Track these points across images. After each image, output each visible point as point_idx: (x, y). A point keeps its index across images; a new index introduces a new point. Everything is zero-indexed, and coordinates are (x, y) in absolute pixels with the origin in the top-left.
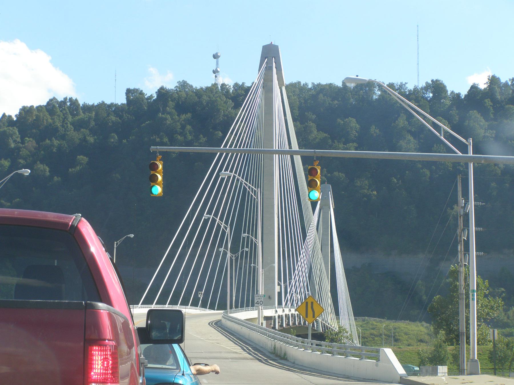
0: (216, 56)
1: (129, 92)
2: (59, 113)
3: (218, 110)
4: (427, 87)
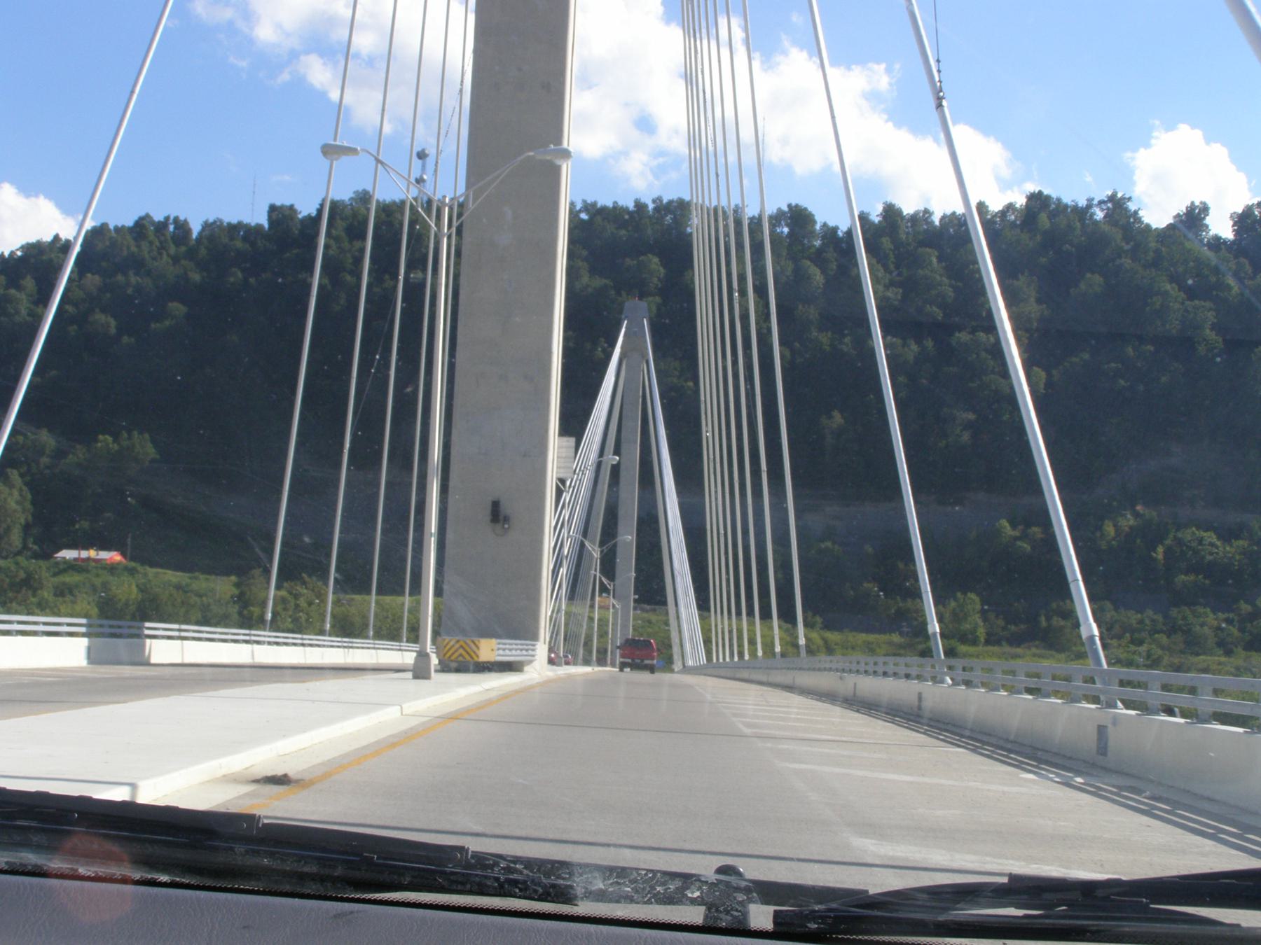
1: (273, 209)
2: (152, 237)
4: (777, 219)
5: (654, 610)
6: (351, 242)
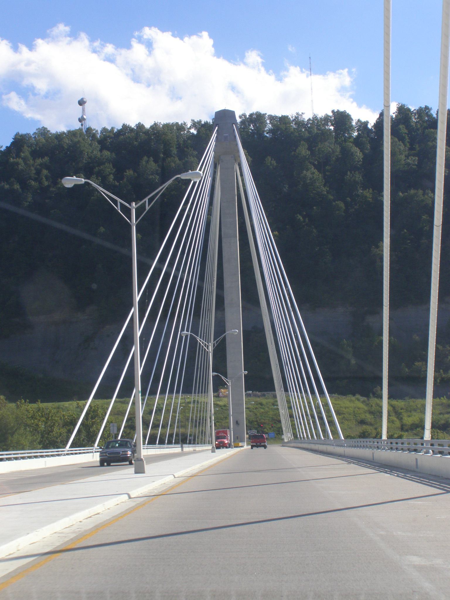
0: (81, 103)
3: (81, 152)
5: (264, 395)
6: (34, 159)
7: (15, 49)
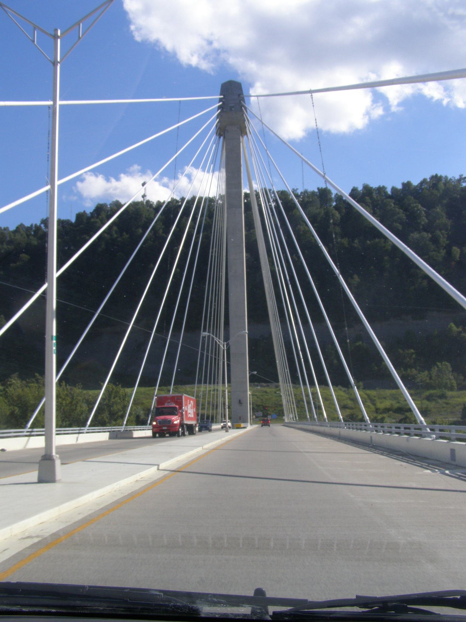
5: (268, 386)
7: (108, 180)
